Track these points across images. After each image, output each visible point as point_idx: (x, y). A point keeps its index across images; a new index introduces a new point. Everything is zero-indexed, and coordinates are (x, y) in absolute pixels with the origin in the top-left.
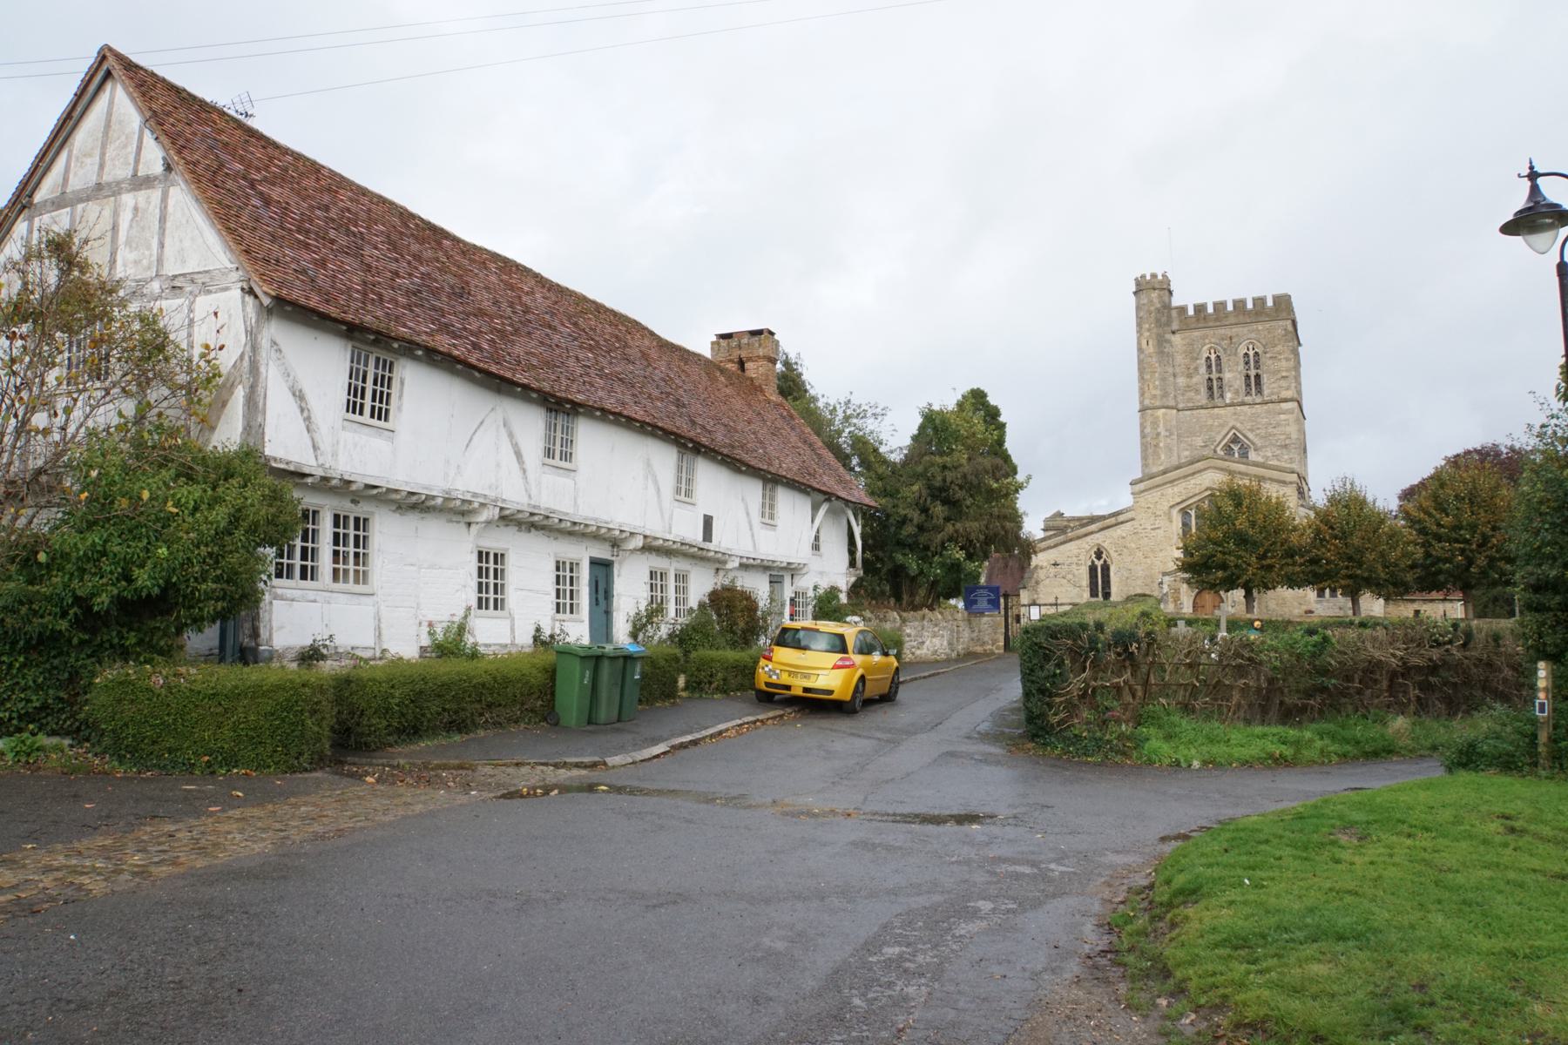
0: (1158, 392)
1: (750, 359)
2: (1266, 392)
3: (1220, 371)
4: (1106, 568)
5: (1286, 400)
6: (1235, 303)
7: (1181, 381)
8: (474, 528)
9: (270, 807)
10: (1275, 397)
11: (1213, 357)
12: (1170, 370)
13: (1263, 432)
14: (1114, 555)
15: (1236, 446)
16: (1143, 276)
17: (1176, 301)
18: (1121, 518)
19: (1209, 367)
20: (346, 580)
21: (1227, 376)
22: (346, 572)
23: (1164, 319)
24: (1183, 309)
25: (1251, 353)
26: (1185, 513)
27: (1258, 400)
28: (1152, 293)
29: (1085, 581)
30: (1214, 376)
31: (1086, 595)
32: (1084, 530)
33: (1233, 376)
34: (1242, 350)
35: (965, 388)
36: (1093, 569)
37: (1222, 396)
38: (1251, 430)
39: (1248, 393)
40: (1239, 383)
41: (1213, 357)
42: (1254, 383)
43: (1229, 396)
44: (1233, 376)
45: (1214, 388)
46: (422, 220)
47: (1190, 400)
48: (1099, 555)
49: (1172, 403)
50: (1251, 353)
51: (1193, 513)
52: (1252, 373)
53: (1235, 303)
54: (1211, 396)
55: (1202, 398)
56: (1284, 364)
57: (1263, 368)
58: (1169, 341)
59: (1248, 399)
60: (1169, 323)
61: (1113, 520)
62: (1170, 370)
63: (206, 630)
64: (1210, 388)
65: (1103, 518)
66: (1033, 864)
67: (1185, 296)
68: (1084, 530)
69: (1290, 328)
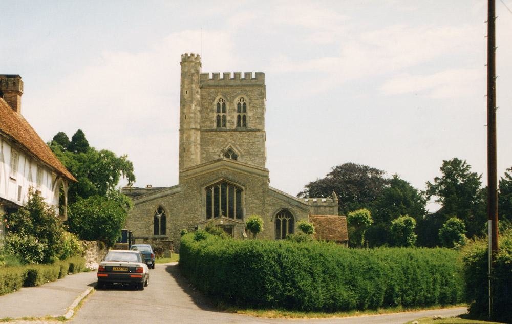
4: (164, 218)
6: (246, 74)
8: (28, 195)
9: (302, 288)
16: (186, 55)
17: (203, 70)
24: (207, 75)
25: (242, 103)
26: (208, 189)
28: (189, 63)
29: (168, 225)
31: (152, 233)
32: (152, 197)
33: (232, 117)
36: (156, 219)
37: (225, 126)
44: (232, 117)
45: (221, 122)
46: (183, 82)
50: (242, 103)
52: (242, 115)
53: (246, 74)
66: (426, 318)
67: (209, 67)
68: (152, 197)
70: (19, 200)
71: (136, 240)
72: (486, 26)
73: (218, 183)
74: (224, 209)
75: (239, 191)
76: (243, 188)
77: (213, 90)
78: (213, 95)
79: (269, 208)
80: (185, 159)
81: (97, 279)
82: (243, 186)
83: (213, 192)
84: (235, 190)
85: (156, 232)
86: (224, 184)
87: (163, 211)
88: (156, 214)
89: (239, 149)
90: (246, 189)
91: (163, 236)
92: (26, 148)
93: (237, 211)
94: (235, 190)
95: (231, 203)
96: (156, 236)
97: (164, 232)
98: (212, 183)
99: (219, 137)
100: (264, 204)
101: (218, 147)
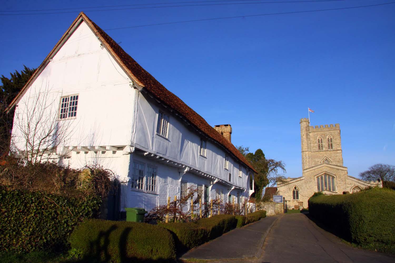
0: (306, 147)
1: (225, 132)
2: (334, 148)
3: (322, 142)
4: (297, 192)
5: (339, 150)
7: (312, 145)
10: (336, 149)
11: (320, 139)
12: (309, 142)
13: (333, 158)
14: (299, 188)
15: (327, 161)
18: (302, 179)
19: (319, 141)
20: (72, 97)
21: (324, 144)
22: (71, 100)
23: (308, 129)
25: (330, 138)
27: (332, 150)
29: (299, 195)
30: (320, 144)
31: (292, 198)
33: (325, 144)
34: (327, 137)
35: (258, 148)
36: (294, 192)
37: (322, 149)
38: (330, 157)
39: (329, 148)
40: (327, 146)
41: (320, 139)
42: (331, 146)
43: (324, 149)
45: (320, 147)
47: (314, 150)
48: (295, 188)
49: (310, 150)
50: (330, 138)
51: (320, 178)
52: (330, 143)
54: (319, 148)
55: (317, 149)
56: (338, 141)
57: (333, 142)
58: (309, 135)
59: (329, 150)
60: (309, 130)
61: (299, 179)
62: (309, 142)
63: (128, 178)
64: (319, 147)
65: (297, 179)
69: (339, 132)
70: (230, 181)
71: (130, 253)
72: (60, 50)
73: (322, 175)
74: (326, 186)
75: (333, 178)
76: (335, 176)
77: (316, 133)
78: (316, 136)
79: (348, 185)
80: (305, 165)
81: (308, 206)
82: (335, 175)
83: (320, 179)
84: (331, 177)
85: (294, 198)
86: (326, 174)
87: (297, 188)
88: (294, 190)
89: (330, 159)
90: (336, 177)
91: (297, 200)
92: (235, 156)
93: (332, 187)
94: (331, 177)
95: (329, 184)
96: (294, 200)
97: (297, 198)
98: (319, 175)
99: (320, 154)
100: (345, 183)
101: (320, 159)
